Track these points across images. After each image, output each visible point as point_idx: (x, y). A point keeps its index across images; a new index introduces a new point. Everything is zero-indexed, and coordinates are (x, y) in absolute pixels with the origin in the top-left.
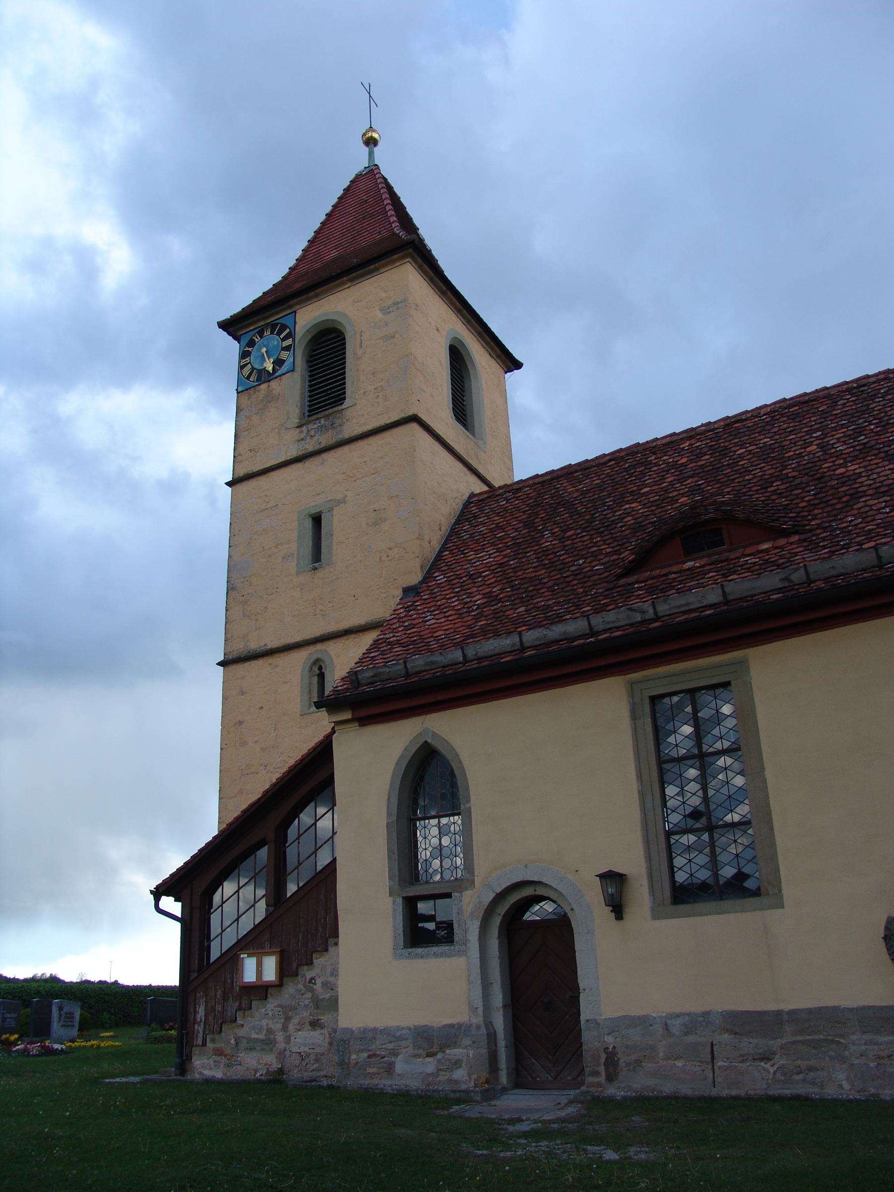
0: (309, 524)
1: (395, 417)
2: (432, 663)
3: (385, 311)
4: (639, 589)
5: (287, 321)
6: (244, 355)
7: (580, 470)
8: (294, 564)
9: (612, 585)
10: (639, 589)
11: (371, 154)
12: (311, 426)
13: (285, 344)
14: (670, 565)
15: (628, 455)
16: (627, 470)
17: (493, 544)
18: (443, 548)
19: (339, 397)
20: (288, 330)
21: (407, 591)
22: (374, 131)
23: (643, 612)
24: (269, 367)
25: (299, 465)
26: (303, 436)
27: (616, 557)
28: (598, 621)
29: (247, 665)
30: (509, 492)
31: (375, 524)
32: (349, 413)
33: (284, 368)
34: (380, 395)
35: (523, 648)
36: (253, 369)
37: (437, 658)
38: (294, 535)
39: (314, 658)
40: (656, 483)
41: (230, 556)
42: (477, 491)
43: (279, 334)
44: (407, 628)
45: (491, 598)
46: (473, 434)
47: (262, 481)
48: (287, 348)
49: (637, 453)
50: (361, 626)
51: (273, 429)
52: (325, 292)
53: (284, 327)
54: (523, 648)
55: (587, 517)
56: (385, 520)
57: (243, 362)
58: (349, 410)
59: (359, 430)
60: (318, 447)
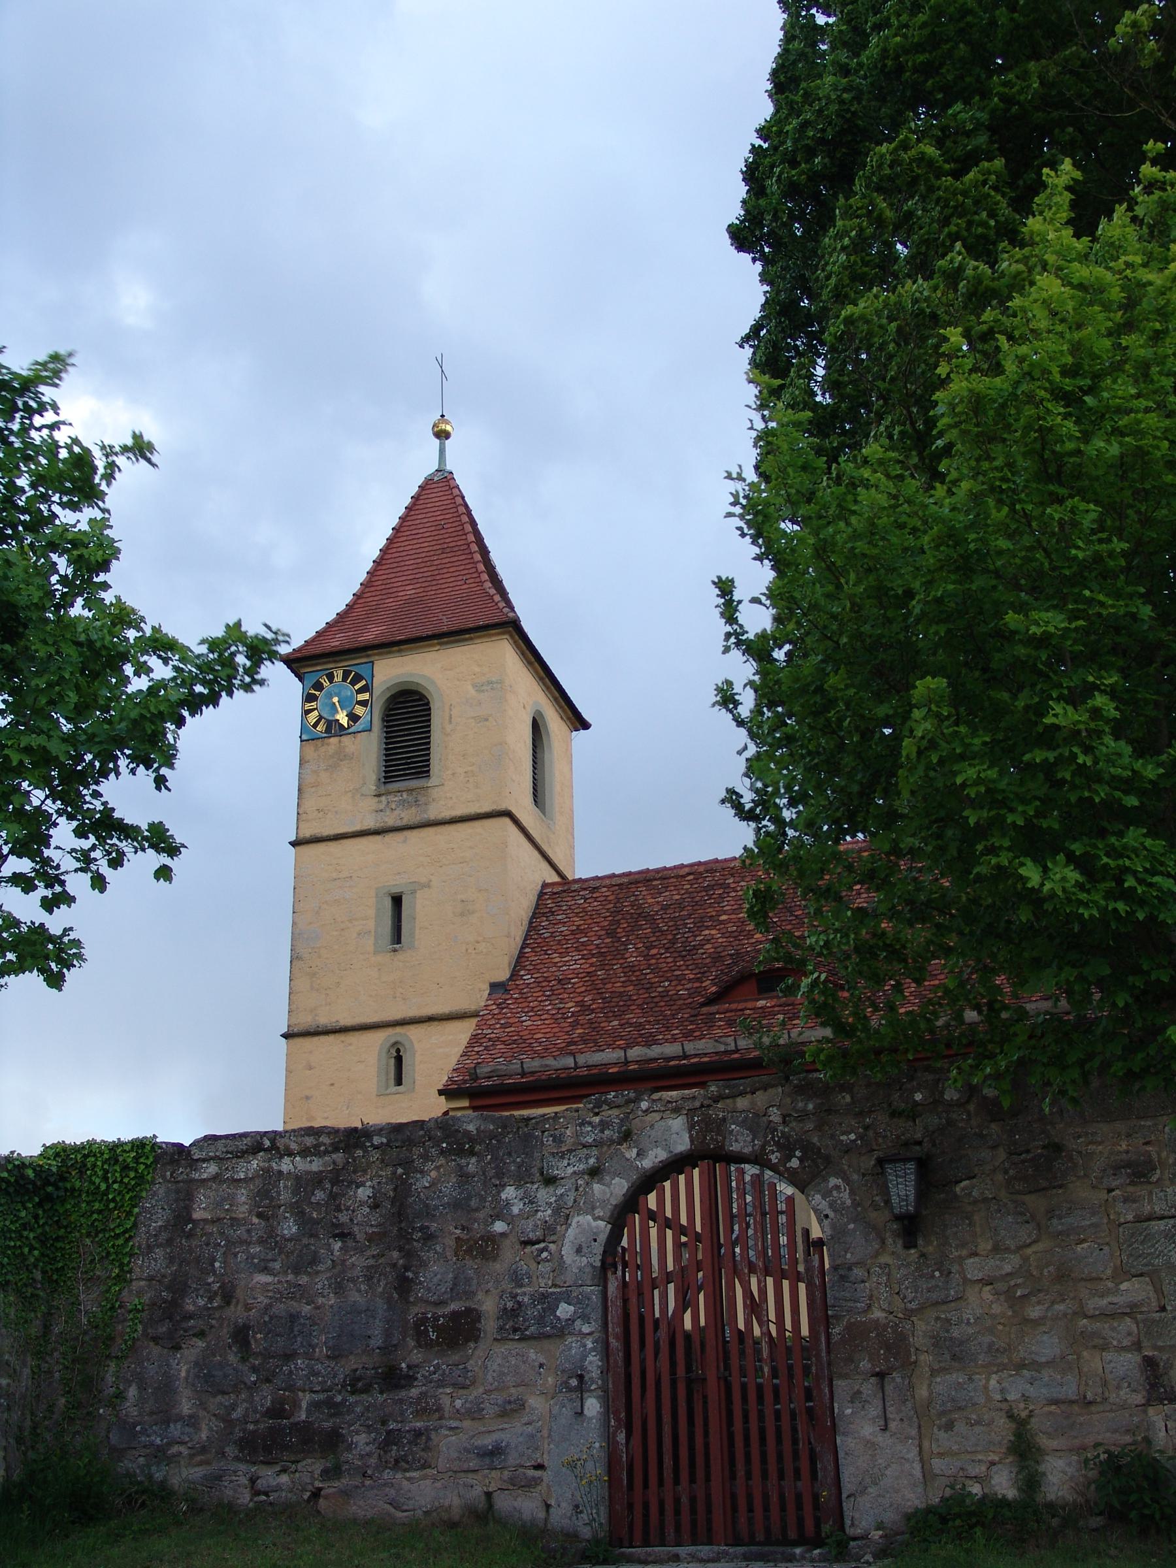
0: (388, 903)
1: (486, 808)
2: (547, 1066)
3: (478, 688)
4: (720, 1019)
5: (363, 670)
6: (309, 698)
7: (660, 879)
8: (371, 941)
9: (696, 1012)
10: (720, 1019)
11: (442, 451)
12: (391, 798)
13: (361, 697)
14: (746, 1001)
15: (707, 871)
16: (706, 889)
17: (577, 950)
18: (524, 945)
19: (423, 770)
20: (363, 683)
21: (494, 986)
22: (447, 422)
23: (726, 1044)
24: (344, 721)
25: (378, 838)
26: (382, 807)
27: (697, 985)
28: (690, 1047)
29: (316, 1039)
30: (585, 889)
31: (462, 914)
32: (434, 793)
33: (359, 725)
34: (471, 780)
35: (627, 1062)
36: (320, 718)
37: (550, 1061)
38: (371, 912)
39: (393, 1040)
40: (734, 912)
41: (294, 924)
42: (549, 881)
43: (353, 683)
44: (504, 1026)
45: (584, 1008)
46: (543, 812)
47: (333, 847)
48: (364, 703)
49: (716, 871)
50: (444, 1014)
51: (346, 792)
52: (411, 649)
53: (358, 678)
54: (627, 1062)
55: (670, 937)
56: (473, 912)
57: (308, 706)
58: (436, 789)
59: (447, 814)
60: (399, 823)
